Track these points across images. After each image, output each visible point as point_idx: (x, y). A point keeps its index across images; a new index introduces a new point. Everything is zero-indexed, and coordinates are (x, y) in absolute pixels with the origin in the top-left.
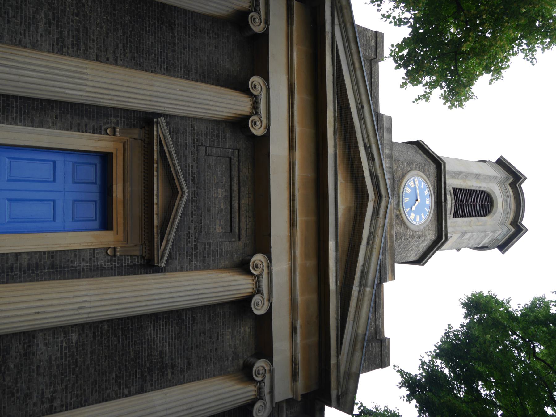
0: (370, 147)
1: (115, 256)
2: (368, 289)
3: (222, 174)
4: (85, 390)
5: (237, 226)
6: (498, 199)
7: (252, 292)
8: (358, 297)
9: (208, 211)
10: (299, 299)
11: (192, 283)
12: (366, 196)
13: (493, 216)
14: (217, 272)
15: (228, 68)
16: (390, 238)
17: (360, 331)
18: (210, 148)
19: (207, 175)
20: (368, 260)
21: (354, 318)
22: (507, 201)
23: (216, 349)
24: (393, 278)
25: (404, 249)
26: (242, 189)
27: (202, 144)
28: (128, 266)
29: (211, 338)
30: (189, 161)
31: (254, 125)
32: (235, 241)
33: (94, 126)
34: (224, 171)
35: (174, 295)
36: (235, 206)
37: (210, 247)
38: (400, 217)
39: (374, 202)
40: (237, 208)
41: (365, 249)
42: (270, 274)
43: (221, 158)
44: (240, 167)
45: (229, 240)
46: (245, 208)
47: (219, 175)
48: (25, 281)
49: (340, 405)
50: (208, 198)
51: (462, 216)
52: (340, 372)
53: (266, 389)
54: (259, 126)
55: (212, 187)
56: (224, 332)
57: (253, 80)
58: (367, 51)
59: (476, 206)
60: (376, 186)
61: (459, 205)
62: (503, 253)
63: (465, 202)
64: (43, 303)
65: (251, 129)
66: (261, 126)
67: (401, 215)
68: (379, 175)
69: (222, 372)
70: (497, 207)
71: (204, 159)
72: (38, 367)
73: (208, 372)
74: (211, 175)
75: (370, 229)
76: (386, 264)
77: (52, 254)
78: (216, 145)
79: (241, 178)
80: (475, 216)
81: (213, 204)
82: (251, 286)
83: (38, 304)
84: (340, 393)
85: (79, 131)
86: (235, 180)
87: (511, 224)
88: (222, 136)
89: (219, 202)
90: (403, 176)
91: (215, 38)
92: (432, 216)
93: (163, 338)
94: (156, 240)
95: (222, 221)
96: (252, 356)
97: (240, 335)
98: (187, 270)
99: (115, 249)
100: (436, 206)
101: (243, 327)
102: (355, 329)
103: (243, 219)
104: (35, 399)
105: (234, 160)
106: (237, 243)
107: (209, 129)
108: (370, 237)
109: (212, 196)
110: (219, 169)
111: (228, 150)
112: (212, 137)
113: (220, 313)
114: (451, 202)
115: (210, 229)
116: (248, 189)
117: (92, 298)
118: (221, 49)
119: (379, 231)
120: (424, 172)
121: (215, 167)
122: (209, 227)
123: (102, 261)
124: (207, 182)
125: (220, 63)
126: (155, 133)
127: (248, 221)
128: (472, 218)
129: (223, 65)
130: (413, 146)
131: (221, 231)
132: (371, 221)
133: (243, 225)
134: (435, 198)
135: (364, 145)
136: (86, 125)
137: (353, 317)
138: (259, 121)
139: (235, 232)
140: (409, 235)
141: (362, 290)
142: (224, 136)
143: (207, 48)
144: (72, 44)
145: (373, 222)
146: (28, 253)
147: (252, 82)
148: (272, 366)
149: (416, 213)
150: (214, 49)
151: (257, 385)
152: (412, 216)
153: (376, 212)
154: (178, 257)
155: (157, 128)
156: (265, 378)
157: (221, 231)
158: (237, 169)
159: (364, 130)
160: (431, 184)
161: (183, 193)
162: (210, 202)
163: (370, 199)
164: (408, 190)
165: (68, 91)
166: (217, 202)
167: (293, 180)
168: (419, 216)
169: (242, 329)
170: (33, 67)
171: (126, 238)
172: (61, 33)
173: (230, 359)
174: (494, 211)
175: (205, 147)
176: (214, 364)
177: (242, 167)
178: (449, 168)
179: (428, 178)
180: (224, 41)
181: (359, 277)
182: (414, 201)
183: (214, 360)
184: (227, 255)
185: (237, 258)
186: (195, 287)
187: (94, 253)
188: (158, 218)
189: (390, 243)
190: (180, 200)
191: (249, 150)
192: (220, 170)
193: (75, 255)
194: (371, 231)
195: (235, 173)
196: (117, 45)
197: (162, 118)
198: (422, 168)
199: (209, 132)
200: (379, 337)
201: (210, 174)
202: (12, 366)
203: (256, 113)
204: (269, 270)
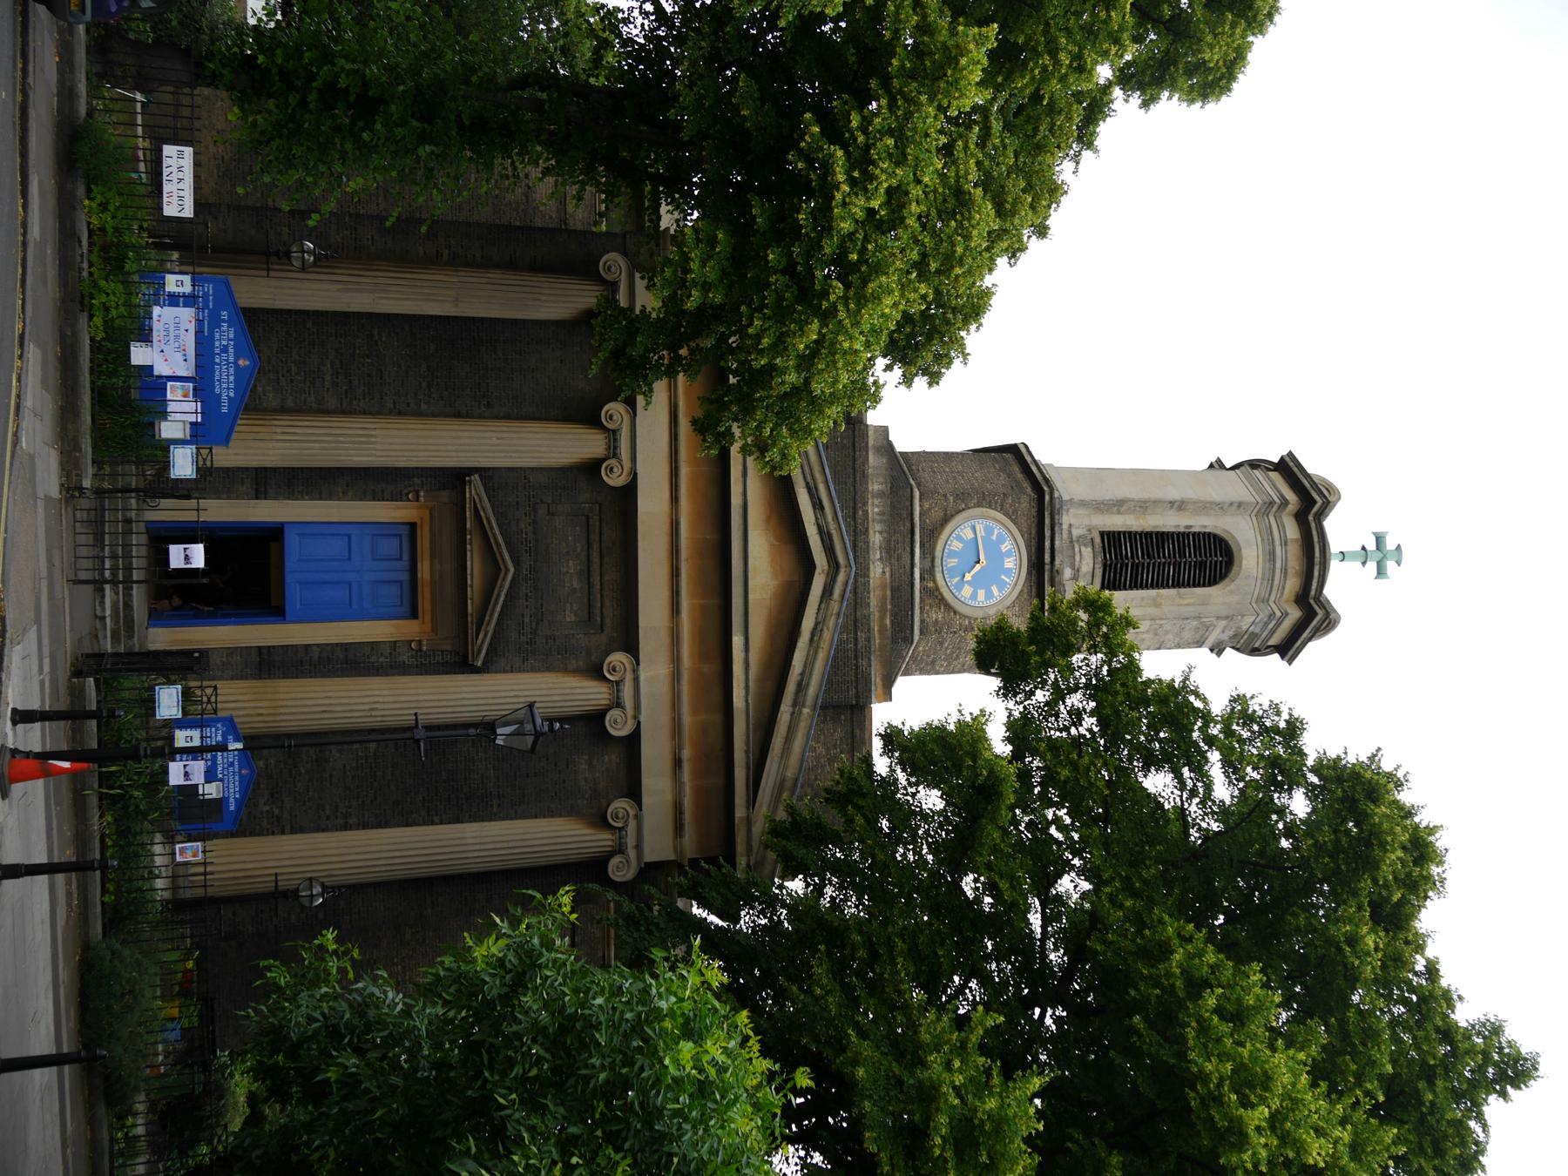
0: (816, 488)
1: (421, 650)
2: (806, 711)
4: (385, 810)
5: (598, 612)
6: (1243, 551)
8: (791, 722)
10: (687, 719)
11: (515, 687)
12: (808, 567)
16: (880, 631)
17: (789, 774)
21: (782, 754)
23: (564, 781)
26: (606, 559)
27: (541, 501)
28: (438, 663)
29: (556, 765)
30: (522, 525)
33: (392, 492)
35: (491, 701)
38: (937, 594)
40: (598, 587)
42: (636, 680)
48: (316, 677)
53: (631, 841)
62: (1290, 662)
63: (1143, 557)
64: (332, 701)
65: (605, 478)
67: (937, 589)
68: (833, 532)
69: (573, 812)
70: (1240, 566)
72: (331, 776)
76: (870, 674)
77: (345, 647)
82: (606, 696)
83: (327, 701)
85: (374, 500)
86: (596, 546)
90: (945, 520)
92: (1022, 591)
93: (486, 759)
94: (470, 631)
98: (520, 672)
99: (420, 642)
100: (1034, 572)
103: (607, 602)
104: (328, 812)
117: (386, 699)
120: (1002, 510)
123: (405, 657)
126: (468, 495)
128: (1162, 591)
131: (573, 618)
136: (383, 491)
140: (960, 624)
144: (364, 395)
145: (823, 606)
146: (318, 645)
147: (607, 412)
148: (641, 810)
149: (975, 584)
152: (967, 591)
154: (507, 654)
155: (470, 488)
157: (573, 618)
158: (597, 530)
160: (1020, 531)
161: (507, 570)
163: (818, 570)
164: (956, 545)
165: (356, 459)
167: (677, 546)
168: (983, 591)
169: (606, 758)
170: (315, 438)
171: (434, 630)
172: (350, 382)
174: (1231, 575)
178: (1064, 490)
179: (1012, 520)
182: (972, 564)
186: (520, 693)
187: (395, 647)
188: (472, 603)
189: (880, 638)
190: (504, 579)
193: (373, 649)
195: (595, 537)
196: (420, 384)
197: (477, 476)
198: (996, 503)
202: (303, 771)
203: (615, 456)
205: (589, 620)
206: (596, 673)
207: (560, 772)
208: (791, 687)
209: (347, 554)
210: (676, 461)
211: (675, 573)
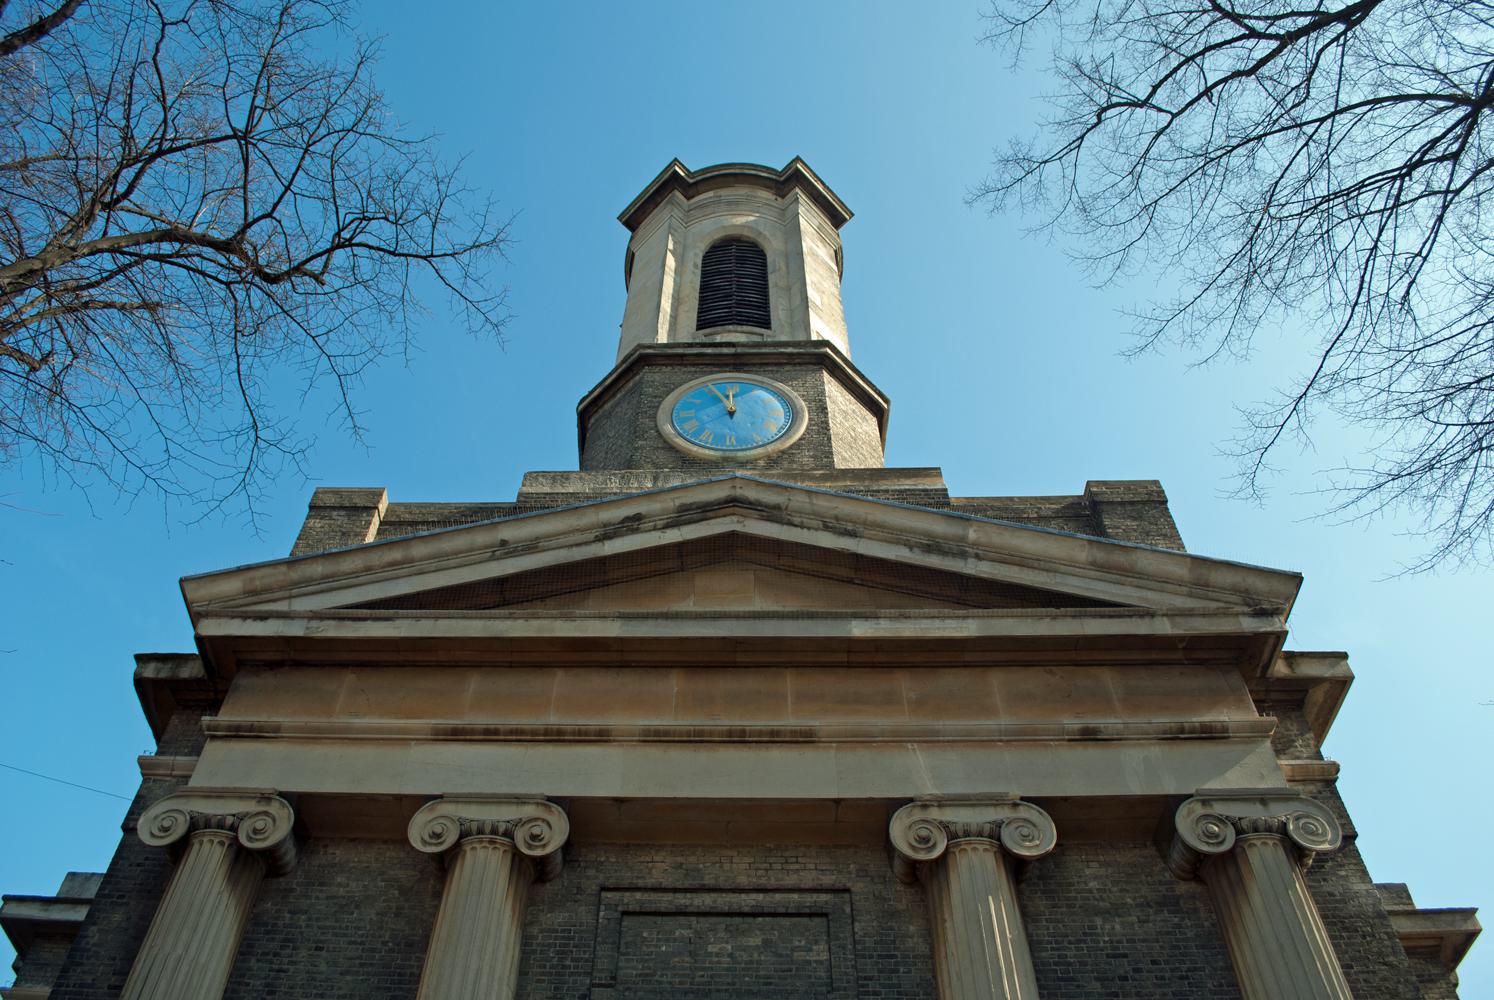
2: (972, 534)
3: (667, 940)
5: (810, 899)
7: (995, 853)
9: (770, 984)
10: (1005, 721)
13: (765, 236)
14: (943, 954)
15: (378, 914)
18: (594, 974)
19: (671, 983)
20: (896, 536)
21: (1047, 571)
22: (729, 203)
23: (1154, 962)
24: (934, 472)
25: (852, 447)
26: (708, 881)
29: (1125, 979)
31: (541, 840)
32: (852, 904)
34: (658, 933)
36: (754, 903)
37: (871, 979)
39: (745, 517)
40: (761, 896)
41: (869, 542)
42: (942, 802)
43: (623, 941)
44: (649, 886)
45: (850, 921)
46: (760, 872)
47: (671, 949)
49: (1278, 609)
50: (734, 984)
51: (765, 308)
52: (1192, 609)
54: (545, 827)
55: (703, 969)
56: (1107, 939)
57: (419, 840)
58: (358, 530)
59: (740, 276)
60: (706, 511)
61: (739, 314)
65: (549, 850)
66: (544, 820)
71: (627, 993)
73: (1221, 985)
74: (669, 973)
75: (816, 530)
78: (587, 956)
79: (678, 885)
80: (764, 277)
81: (748, 969)
84: (1246, 609)
86: (682, 900)
87: (783, 197)
88: (563, 938)
89: (744, 950)
91: (294, 948)
92: (770, 378)
95: (797, 943)
96: (1165, 856)
97: (1111, 892)
101: (1086, 883)
102: (1077, 570)
103: (790, 880)
105: (628, 904)
106: (858, 898)
107: (543, 974)
108: (836, 528)
109: (728, 969)
110: (653, 949)
111: (600, 921)
112: (564, 967)
113: (1052, 949)
114: (734, 334)
115: (820, 978)
116: (708, 864)
118: (324, 933)
119: (822, 503)
121: (646, 961)
122: (813, 980)
124: (688, 986)
125: (362, 936)
127: (797, 866)
128: (771, 285)
129: (368, 927)
130: (593, 424)
132: (796, 526)
133: (809, 879)
134: (726, 372)
135: (599, 540)
137: (1045, 574)
138: (530, 825)
139: (826, 903)
141: (975, 551)
142: (563, 931)
143: (321, 973)
150: (324, 953)
151: (1246, 840)
153: (771, 513)
156: (1227, 817)
157: (822, 946)
158: (653, 896)
159: (563, 541)
162: (744, 976)
163: (738, 528)
166: (745, 957)
167: (688, 734)
173: (1176, 919)
174: (752, 235)
175: (593, 989)
176: (1195, 969)
177: (650, 882)
180: (304, 925)
181: (940, 557)
183: (1184, 967)
184: (891, 928)
185: (901, 897)
191: (602, 859)
192: (656, 946)
194: (821, 526)
195: (665, 901)
199: (551, 974)
200: (1085, 508)
201: (666, 975)
204: (933, 805)
205: (825, 915)
206: (444, 863)
207: (1137, 970)
208: (934, 561)
209: (817, 920)
210: (534, 732)
211: (738, 738)
